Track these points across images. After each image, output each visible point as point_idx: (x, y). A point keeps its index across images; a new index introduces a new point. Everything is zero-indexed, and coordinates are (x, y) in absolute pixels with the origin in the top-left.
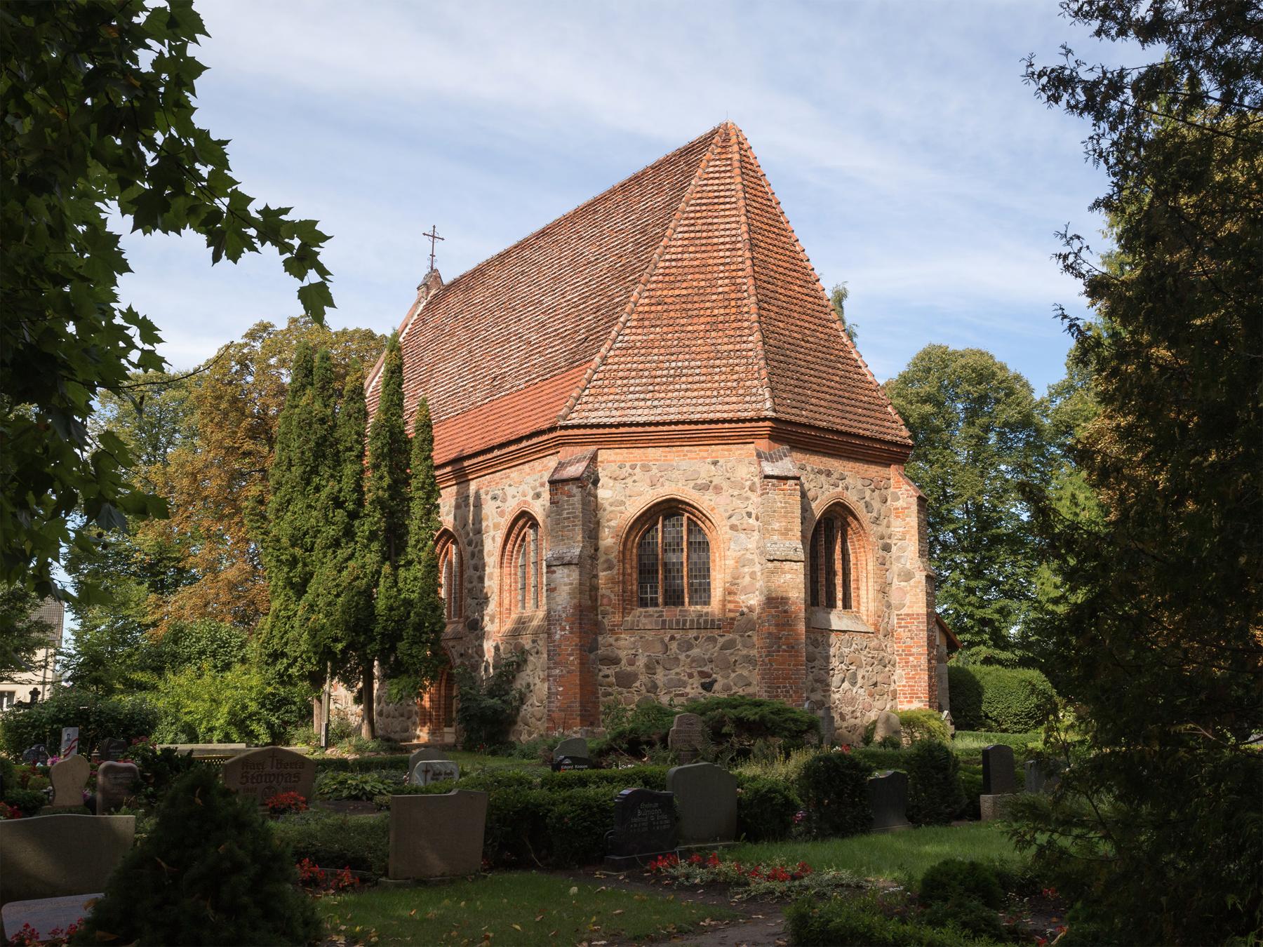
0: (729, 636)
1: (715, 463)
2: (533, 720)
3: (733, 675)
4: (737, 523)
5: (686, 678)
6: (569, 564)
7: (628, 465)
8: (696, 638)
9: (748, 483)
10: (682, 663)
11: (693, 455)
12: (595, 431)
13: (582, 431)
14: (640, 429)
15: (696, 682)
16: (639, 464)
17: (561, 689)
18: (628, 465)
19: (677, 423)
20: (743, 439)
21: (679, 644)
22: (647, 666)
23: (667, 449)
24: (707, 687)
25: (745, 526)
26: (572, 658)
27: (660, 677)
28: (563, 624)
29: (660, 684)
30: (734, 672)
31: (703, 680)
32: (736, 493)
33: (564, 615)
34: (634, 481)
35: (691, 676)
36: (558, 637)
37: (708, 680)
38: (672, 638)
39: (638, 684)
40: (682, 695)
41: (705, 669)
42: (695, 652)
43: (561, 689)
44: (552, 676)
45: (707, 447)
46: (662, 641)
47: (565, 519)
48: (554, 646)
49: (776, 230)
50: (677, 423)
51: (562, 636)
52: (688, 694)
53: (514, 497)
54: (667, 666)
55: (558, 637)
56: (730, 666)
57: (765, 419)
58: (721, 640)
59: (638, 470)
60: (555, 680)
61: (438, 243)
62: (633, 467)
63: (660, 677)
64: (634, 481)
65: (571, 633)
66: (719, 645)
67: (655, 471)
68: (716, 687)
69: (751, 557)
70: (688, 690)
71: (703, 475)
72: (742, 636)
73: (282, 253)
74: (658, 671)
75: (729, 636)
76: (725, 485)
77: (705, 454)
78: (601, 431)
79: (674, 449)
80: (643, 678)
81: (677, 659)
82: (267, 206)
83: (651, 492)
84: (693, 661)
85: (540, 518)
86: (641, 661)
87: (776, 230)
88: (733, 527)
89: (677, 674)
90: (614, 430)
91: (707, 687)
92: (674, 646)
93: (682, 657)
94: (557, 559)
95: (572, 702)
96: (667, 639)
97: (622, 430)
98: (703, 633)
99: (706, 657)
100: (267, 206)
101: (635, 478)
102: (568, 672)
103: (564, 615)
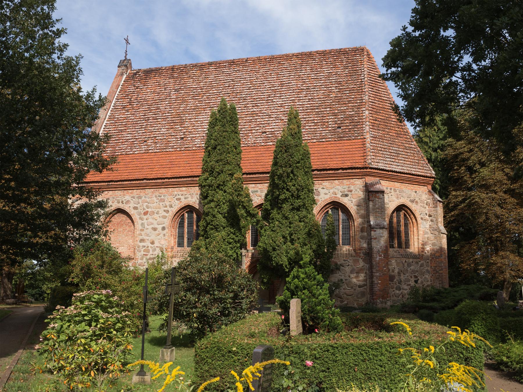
0: (422, 262)
1: (416, 192)
2: (345, 296)
3: (423, 277)
4: (423, 217)
5: (410, 278)
6: (383, 228)
7: (389, 188)
8: (412, 262)
9: (426, 202)
10: (409, 272)
11: (409, 188)
12: (381, 172)
13: (376, 171)
14: (395, 174)
15: (413, 280)
16: (393, 188)
17: (380, 282)
18: (389, 188)
19: (407, 174)
20: (424, 184)
21: (407, 264)
22: (399, 273)
23: (401, 184)
24: (416, 282)
25: (425, 219)
26: (385, 269)
27: (402, 277)
28: (380, 254)
29: (403, 280)
30: (424, 276)
31: (415, 279)
32: (422, 205)
33: (381, 250)
34: (391, 195)
35: (411, 277)
36: (378, 259)
37: (417, 279)
38: (406, 262)
39: (395, 280)
40: (409, 285)
41: (416, 275)
42: (412, 267)
43: (380, 282)
44: (375, 276)
45: (413, 185)
46: (402, 262)
47: (377, 208)
48: (376, 263)
49: (354, 94)
50: (407, 174)
51: (380, 259)
52: (410, 284)
53: (326, 194)
54: (405, 273)
55: (378, 259)
56: (423, 274)
57: (432, 178)
58: (420, 263)
59: (392, 191)
60: (377, 278)
61: (128, 46)
62: (391, 189)
63: (402, 277)
64: (391, 195)
65: (384, 258)
66: (419, 265)
67: (398, 192)
68: (419, 282)
69: (427, 231)
70: (410, 283)
71: (413, 196)
72: (425, 262)
73: (395, 84)
74: (402, 275)
75: (422, 262)
76: (419, 201)
77: (412, 188)
78: (383, 172)
79: (403, 184)
80: (397, 278)
81: (407, 270)
82: (382, 59)
83: (397, 200)
84: (412, 271)
85: (353, 209)
86: (396, 271)
87: (354, 94)
88: (422, 219)
89: (408, 276)
90: (387, 173)
91: (416, 282)
92: (406, 265)
93: (409, 269)
94: (377, 225)
95: (385, 287)
96: (404, 262)
97: (390, 173)
98: (415, 260)
99: (416, 270)
100: (382, 59)
101: (391, 194)
102: (383, 275)
103: (381, 250)
